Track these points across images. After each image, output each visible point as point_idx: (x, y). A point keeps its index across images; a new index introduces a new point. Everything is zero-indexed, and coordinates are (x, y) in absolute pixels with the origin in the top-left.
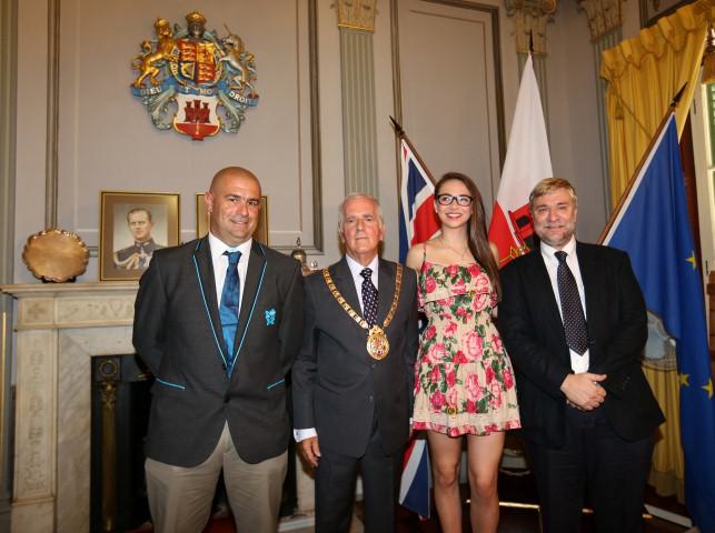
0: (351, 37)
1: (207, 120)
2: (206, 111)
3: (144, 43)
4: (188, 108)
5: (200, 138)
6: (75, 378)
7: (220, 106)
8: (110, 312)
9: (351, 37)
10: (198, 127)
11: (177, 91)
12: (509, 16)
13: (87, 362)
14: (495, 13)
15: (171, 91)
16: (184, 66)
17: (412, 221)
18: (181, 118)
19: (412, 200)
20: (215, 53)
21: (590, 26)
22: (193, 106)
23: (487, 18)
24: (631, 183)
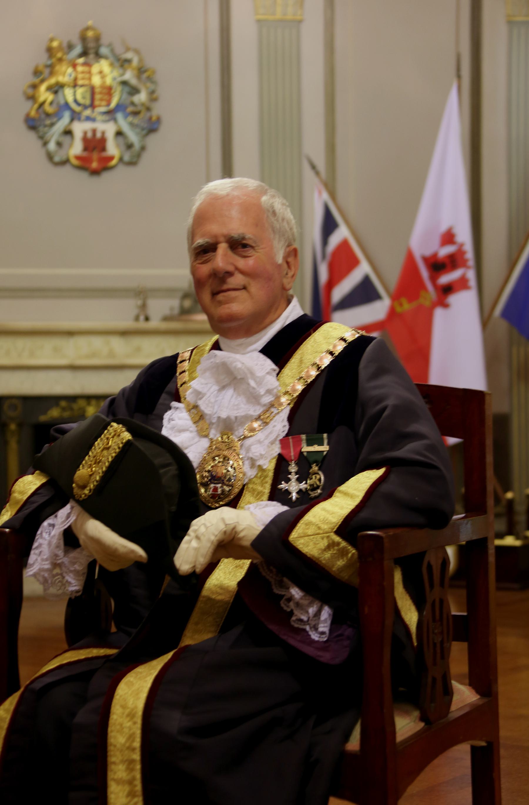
4: (85, 139)
11: (72, 120)
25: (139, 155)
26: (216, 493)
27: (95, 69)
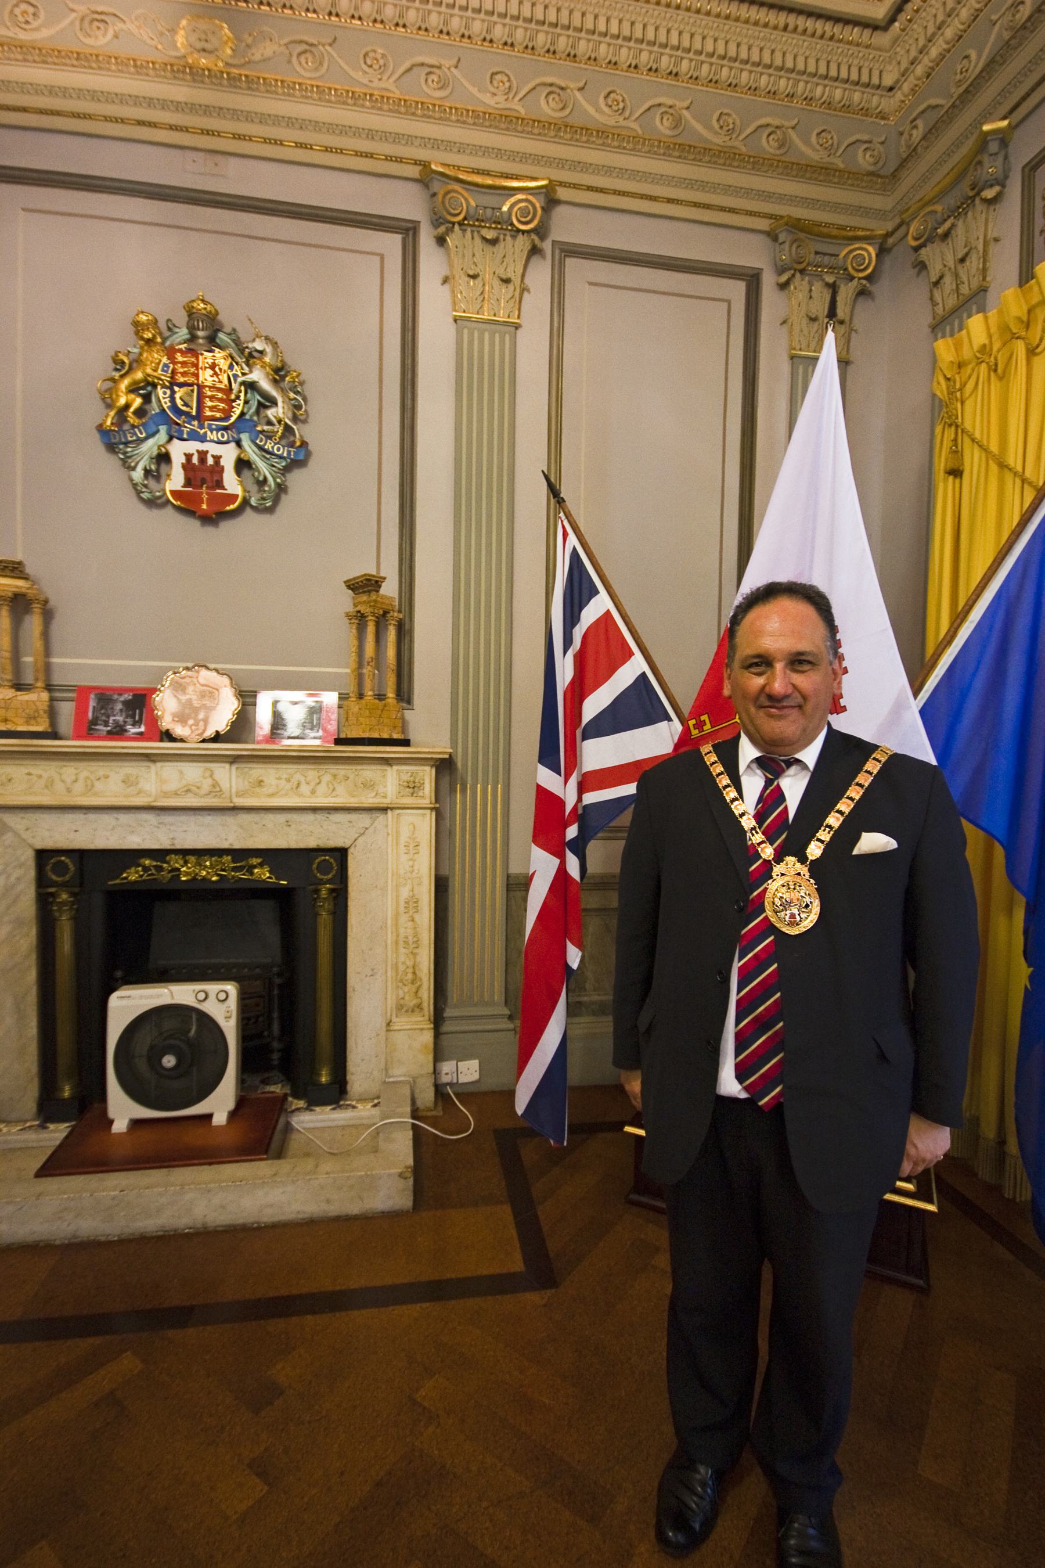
0: (487, 336)
1: (219, 484)
2: (218, 468)
3: (117, 353)
4: (188, 466)
5: (308, 454)
6: (13, 879)
7: (242, 465)
8: (59, 786)
9: (487, 336)
10: (205, 497)
11: (171, 438)
12: (783, 286)
13: (28, 857)
14: (753, 280)
15: (162, 436)
16: (180, 392)
17: (570, 653)
18: (176, 480)
19: (571, 618)
20: (231, 367)
21: (931, 299)
22: (195, 460)
23: (737, 290)
24: (959, 618)
25: (276, 500)
26: (932, 1171)
27: (206, 358)
